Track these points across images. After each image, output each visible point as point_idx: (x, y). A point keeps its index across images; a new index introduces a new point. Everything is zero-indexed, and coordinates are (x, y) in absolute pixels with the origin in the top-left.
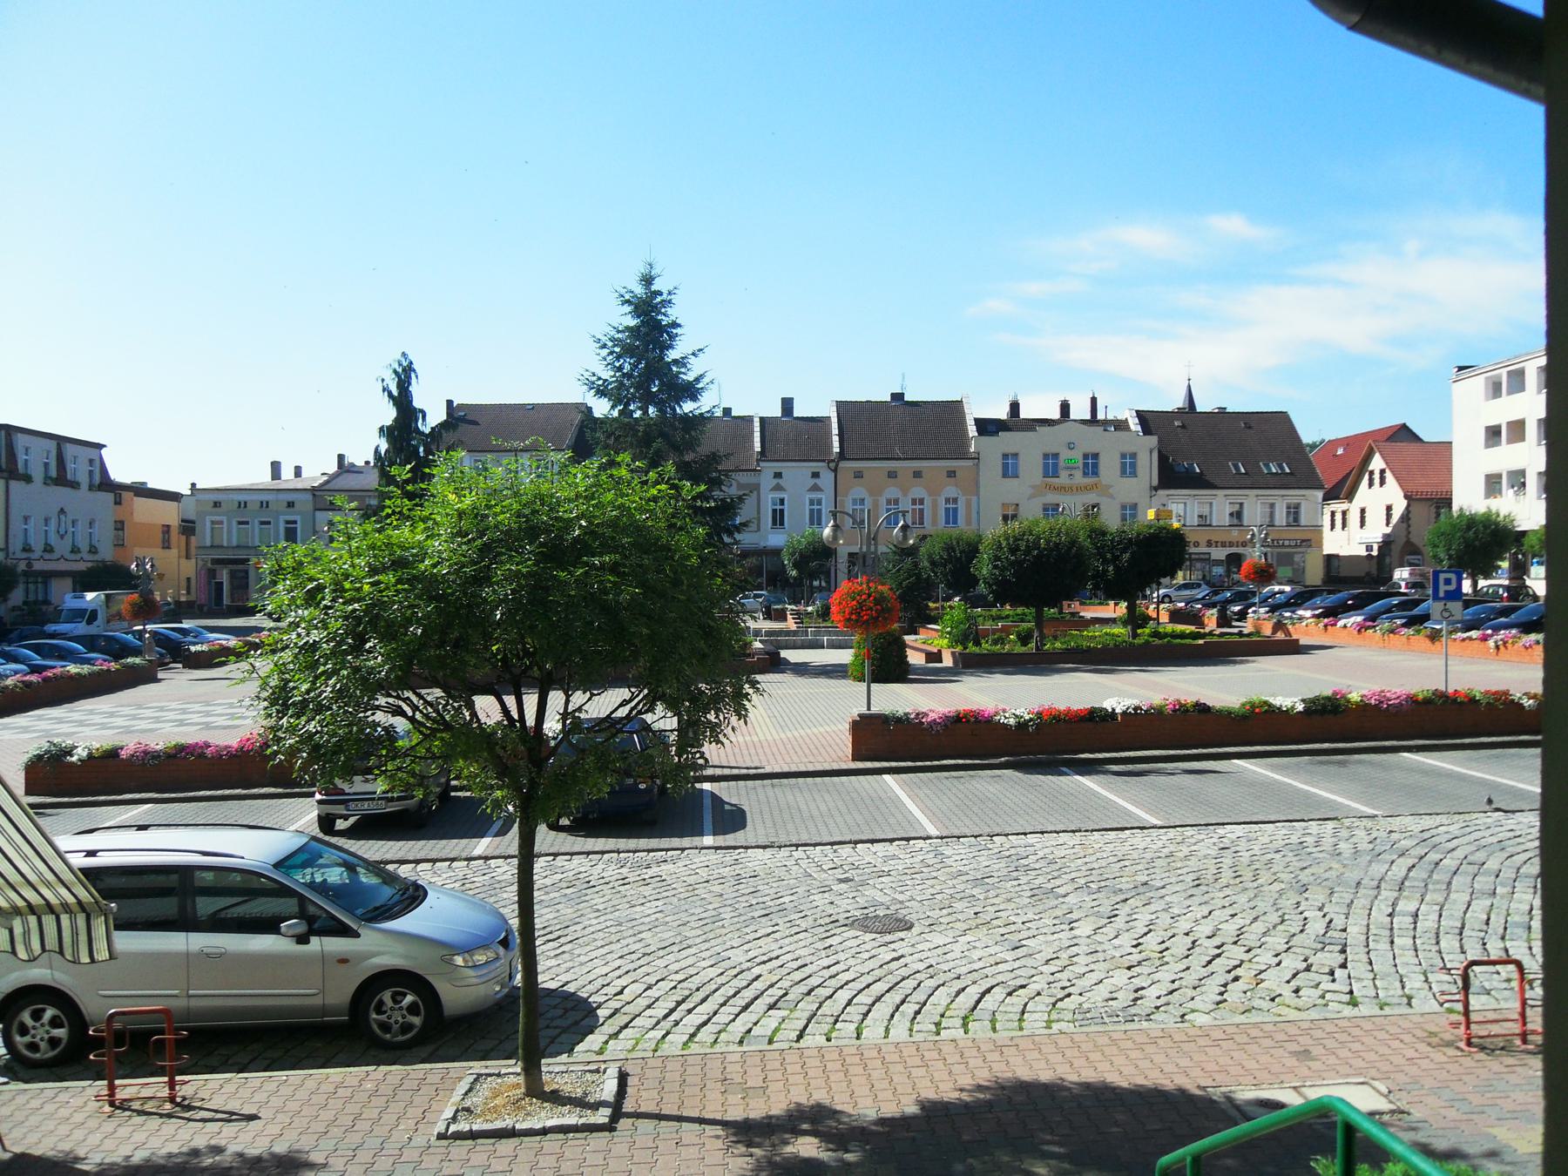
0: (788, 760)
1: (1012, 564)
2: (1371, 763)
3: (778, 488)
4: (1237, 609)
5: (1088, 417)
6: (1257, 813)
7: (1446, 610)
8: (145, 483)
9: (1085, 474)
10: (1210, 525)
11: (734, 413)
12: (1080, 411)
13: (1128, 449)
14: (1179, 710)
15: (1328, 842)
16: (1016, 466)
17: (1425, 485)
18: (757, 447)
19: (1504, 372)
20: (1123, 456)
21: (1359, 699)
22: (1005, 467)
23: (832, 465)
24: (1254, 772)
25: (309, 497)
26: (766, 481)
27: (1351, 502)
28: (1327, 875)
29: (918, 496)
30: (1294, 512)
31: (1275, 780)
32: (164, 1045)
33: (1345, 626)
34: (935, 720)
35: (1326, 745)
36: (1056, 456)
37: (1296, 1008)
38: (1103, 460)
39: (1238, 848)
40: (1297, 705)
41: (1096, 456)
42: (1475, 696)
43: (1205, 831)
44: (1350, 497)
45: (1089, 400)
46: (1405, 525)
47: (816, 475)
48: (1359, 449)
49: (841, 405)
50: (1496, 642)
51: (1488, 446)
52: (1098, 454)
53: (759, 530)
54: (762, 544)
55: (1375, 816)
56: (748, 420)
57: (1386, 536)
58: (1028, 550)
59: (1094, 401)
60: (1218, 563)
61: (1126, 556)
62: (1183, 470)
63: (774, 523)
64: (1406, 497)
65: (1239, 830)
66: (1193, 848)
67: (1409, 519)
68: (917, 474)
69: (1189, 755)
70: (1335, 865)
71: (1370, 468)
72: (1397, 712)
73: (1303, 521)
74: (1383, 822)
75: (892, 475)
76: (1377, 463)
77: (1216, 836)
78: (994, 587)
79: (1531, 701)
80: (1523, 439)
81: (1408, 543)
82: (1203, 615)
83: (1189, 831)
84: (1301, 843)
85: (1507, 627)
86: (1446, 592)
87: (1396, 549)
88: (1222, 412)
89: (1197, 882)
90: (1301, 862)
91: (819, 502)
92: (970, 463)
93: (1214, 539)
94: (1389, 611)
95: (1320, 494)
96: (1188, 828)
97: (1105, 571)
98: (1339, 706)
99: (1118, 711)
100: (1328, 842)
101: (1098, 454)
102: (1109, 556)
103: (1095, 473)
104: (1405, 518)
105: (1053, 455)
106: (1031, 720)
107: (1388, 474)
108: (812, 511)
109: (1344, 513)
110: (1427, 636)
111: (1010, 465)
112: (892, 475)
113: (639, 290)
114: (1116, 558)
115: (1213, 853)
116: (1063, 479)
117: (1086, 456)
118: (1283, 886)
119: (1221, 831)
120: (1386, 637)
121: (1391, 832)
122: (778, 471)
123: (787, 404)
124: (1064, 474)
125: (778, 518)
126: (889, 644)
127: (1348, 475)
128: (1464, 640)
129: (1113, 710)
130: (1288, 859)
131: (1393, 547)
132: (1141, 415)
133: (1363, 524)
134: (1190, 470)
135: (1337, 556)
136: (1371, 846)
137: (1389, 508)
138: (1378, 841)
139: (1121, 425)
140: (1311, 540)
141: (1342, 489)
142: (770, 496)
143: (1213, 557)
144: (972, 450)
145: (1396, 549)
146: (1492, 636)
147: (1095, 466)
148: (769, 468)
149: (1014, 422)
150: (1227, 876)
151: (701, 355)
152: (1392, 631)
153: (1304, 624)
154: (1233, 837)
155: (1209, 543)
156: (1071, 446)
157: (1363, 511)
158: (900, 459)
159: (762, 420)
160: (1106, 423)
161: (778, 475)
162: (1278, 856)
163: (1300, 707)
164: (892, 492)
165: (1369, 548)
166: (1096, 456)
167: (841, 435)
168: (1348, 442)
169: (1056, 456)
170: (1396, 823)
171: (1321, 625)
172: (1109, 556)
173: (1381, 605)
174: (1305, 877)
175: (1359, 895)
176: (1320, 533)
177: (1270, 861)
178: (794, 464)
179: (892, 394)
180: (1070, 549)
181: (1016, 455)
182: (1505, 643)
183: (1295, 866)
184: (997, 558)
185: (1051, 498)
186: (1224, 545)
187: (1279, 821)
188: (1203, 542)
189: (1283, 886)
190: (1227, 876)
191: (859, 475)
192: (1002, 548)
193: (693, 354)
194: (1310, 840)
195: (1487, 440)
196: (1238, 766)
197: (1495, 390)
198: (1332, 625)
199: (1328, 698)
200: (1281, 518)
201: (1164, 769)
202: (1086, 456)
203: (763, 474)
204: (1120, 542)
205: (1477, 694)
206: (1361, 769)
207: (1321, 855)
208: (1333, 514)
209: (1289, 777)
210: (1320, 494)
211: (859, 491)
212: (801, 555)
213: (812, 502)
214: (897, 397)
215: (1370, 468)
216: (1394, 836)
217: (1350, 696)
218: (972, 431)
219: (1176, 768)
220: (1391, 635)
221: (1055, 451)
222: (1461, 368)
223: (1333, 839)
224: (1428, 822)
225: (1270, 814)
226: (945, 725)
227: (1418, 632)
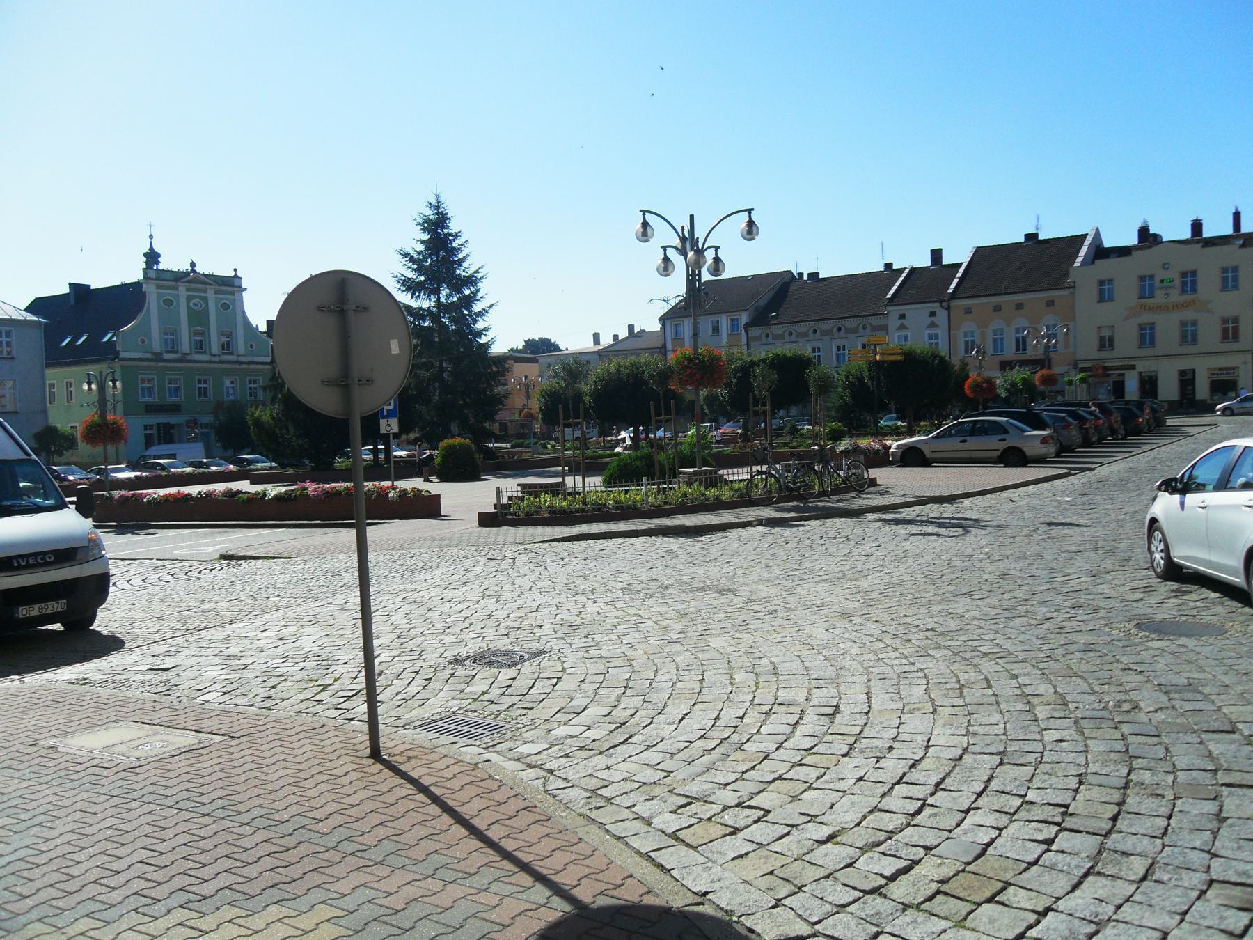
3: (902, 327)
8: (89, 286)
9: (1183, 291)
16: (1111, 291)
20: (1225, 270)
22: (1101, 292)
23: (945, 304)
25: (597, 357)
26: (893, 321)
32: (367, 511)
36: (1152, 277)
37: (1034, 803)
45: (1231, 218)
47: (933, 314)
52: (1196, 271)
59: (1237, 216)
68: (1019, 306)
91: (937, 337)
92: (1066, 292)
101: (1196, 271)
103: (1194, 290)
105: (1223, 273)
111: (1105, 292)
112: (997, 308)
116: (1160, 297)
122: (934, 310)
124: (1159, 295)
142: (896, 334)
148: (895, 311)
151: (491, 311)
156: (1165, 267)
164: (997, 323)
178: (914, 306)
179: (1026, 235)
185: (1146, 318)
191: (968, 311)
202: (1184, 274)
211: (968, 325)
213: (930, 337)
214: (1032, 237)
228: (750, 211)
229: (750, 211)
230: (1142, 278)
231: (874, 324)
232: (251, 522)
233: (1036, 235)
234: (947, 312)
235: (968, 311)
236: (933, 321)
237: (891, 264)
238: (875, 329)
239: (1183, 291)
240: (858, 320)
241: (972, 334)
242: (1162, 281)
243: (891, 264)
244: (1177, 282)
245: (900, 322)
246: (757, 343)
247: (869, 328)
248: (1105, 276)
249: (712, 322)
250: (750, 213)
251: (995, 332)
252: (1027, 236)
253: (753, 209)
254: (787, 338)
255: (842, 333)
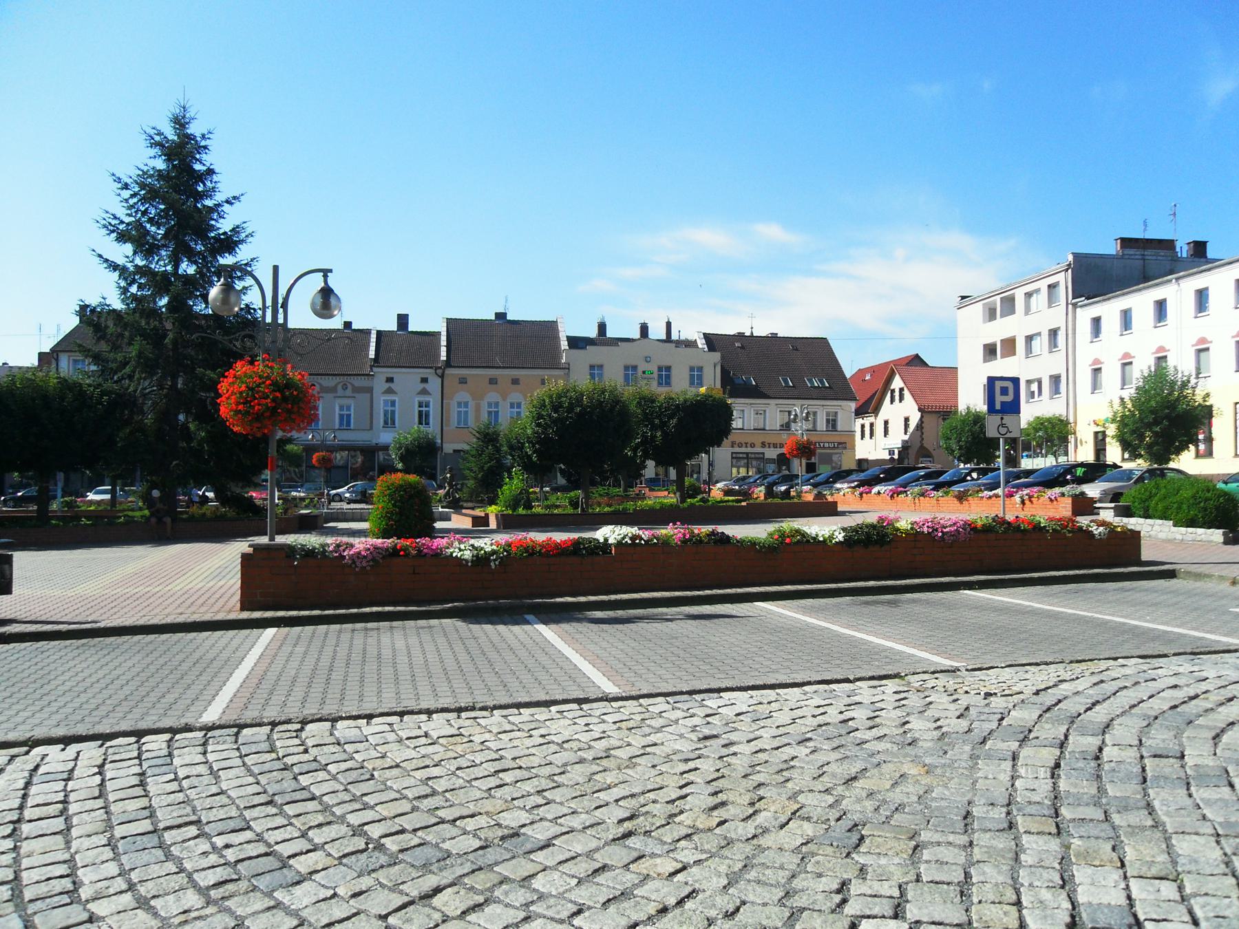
0: (471, 643)
1: (555, 421)
2: (927, 602)
3: (390, 391)
4: (783, 488)
5: (665, 338)
6: (776, 671)
7: (1003, 425)
9: (660, 384)
10: (764, 429)
11: (354, 327)
12: (657, 332)
13: (695, 363)
14: (690, 540)
15: (890, 717)
17: (933, 401)
18: (372, 354)
19: (998, 298)
20: (692, 369)
21: (910, 526)
23: (439, 372)
24: (781, 615)
26: (379, 384)
27: (876, 416)
28: (897, 796)
29: (515, 401)
30: (832, 423)
31: (808, 624)
33: (879, 493)
34: (359, 553)
35: (871, 583)
36: (635, 368)
38: (674, 372)
39: (733, 737)
40: (836, 533)
41: (668, 369)
42: (1040, 522)
43: (686, 703)
44: (876, 411)
46: (919, 433)
47: (424, 380)
48: (886, 373)
49: (451, 323)
50: (1021, 497)
51: (985, 361)
53: (371, 428)
54: (374, 442)
55: (954, 671)
56: (367, 332)
57: (904, 442)
58: (570, 409)
59: (669, 325)
60: (771, 461)
61: (674, 422)
62: (741, 382)
63: (386, 423)
64: (920, 410)
65: (742, 700)
66: (653, 738)
67: (922, 428)
68: (515, 381)
69: (699, 596)
70: (913, 770)
71: (892, 387)
72: (954, 541)
73: (839, 428)
74: (970, 678)
75: (493, 381)
76: (897, 383)
77: (701, 712)
78: (537, 446)
79: (1101, 529)
80: (1014, 354)
81: (922, 447)
82: (753, 492)
83: (660, 704)
84: (845, 721)
85: (1027, 486)
86: (1003, 403)
87: (912, 453)
88: (774, 337)
89: (628, 825)
90: (846, 765)
93: (767, 441)
94: (918, 480)
95: (853, 405)
96: (661, 699)
97: (653, 437)
98: (886, 535)
99: (611, 541)
100: (890, 717)
102: (657, 421)
103: (668, 384)
104: (920, 426)
106: (493, 552)
107: (906, 392)
108: (420, 412)
109: (872, 425)
110: (956, 497)
112: (493, 381)
113: (171, 135)
114: (664, 424)
115: (685, 747)
117: (660, 369)
118: (809, 829)
119: (712, 702)
120: (917, 501)
121: (988, 695)
122: (391, 376)
123: (403, 320)
125: (390, 422)
126: (411, 497)
127: (874, 395)
128: (990, 497)
129: (606, 540)
130: (821, 758)
131: (910, 451)
132: (707, 337)
133: (886, 433)
134: (747, 383)
135: (866, 460)
136: (964, 724)
137: (907, 420)
138: (973, 711)
139: (690, 344)
140: (846, 444)
141: (869, 407)
142: (382, 398)
143: (766, 457)
144: (563, 361)
145: (912, 453)
146: (1017, 492)
147: (668, 377)
148: (382, 373)
149: (601, 337)
150: (695, 811)
151: (237, 204)
152: (923, 495)
153: (842, 493)
154: (728, 712)
155: (763, 445)
156: (647, 360)
157: (886, 423)
158: (500, 367)
159: (379, 333)
160: (679, 343)
161: (390, 380)
162: (802, 751)
163: (840, 537)
164: (492, 396)
165: (891, 452)
166: (668, 369)
167: (448, 346)
168: (873, 370)
169: (635, 368)
170: (991, 680)
171: (857, 493)
172: (657, 421)
173: (910, 477)
174: (855, 804)
175: (977, 853)
176: (854, 440)
177: (788, 764)
178: (404, 370)
180: (613, 408)
181: (601, 367)
182: (1030, 497)
183: (834, 775)
184: (540, 416)
186: (775, 446)
187: (809, 683)
188: (758, 443)
189: (809, 829)
190: (695, 811)
191: (463, 381)
192: (545, 406)
193: (228, 202)
194: (860, 714)
195: (984, 356)
196: (762, 609)
197: (991, 314)
198: (867, 493)
199: (873, 526)
200: (822, 425)
201: (663, 614)
203: (376, 380)
204: (667, 409)
205: (1042, 520)
206: (917, 609)
207: (881, 746)
208: (863, 426)
209: (825, 620)
210: (853, 405)
211: (463, 395)
212: (407, 450)
214: (501, 316)
215: (892, 387)
216: (998, 703)
217: (898, 525)
218: (564, 344)
219: (679, 614)
220: (922, 498)
221: (634, 363)
222: (963, 298)
223: (899, 713)
224: (1040, 677)
225: (796, 671)
226: (373, 559)
227: (947, 493)
228: (326, 272)
229: (326, 272)
230: (626, 368)
231: (356, 384)
232: (1082, 572)
233: (505, 314)
234: (440, 380)
235: (463, 381)
236: (424, 389)
237: (351, 323)
238: (357, 390)
239: (660, 384)
240: (338, 379)
241: (466, 405)
242: (644, 372)
243: (351, 323)
244: (655, 375)
245: (388, 385)
246: (330, 395)
247: (350, 387)
248: (596, 361)
249: (828, 414)
250: (325, 277)
251: (490, 405)
252: (497, 314)
253: (331, 271)
254: (340, 392)
255: (349, 392)
